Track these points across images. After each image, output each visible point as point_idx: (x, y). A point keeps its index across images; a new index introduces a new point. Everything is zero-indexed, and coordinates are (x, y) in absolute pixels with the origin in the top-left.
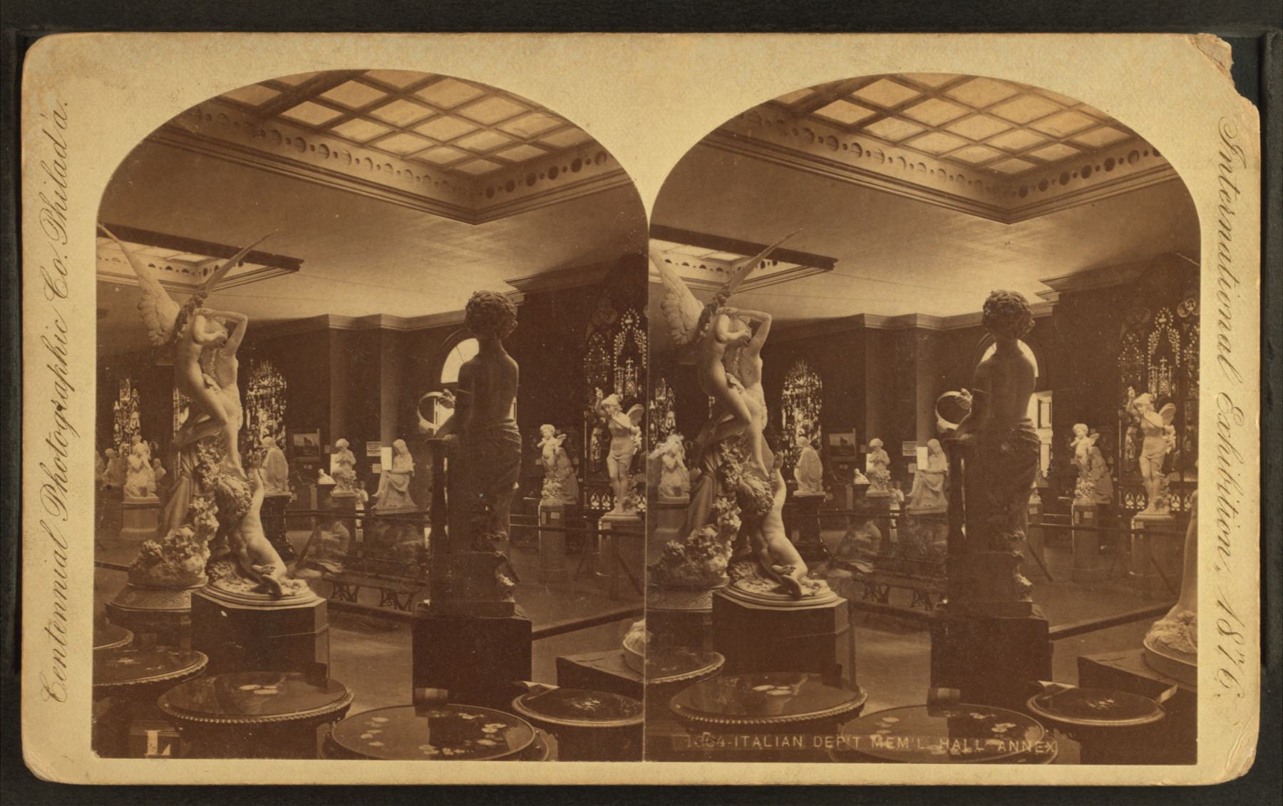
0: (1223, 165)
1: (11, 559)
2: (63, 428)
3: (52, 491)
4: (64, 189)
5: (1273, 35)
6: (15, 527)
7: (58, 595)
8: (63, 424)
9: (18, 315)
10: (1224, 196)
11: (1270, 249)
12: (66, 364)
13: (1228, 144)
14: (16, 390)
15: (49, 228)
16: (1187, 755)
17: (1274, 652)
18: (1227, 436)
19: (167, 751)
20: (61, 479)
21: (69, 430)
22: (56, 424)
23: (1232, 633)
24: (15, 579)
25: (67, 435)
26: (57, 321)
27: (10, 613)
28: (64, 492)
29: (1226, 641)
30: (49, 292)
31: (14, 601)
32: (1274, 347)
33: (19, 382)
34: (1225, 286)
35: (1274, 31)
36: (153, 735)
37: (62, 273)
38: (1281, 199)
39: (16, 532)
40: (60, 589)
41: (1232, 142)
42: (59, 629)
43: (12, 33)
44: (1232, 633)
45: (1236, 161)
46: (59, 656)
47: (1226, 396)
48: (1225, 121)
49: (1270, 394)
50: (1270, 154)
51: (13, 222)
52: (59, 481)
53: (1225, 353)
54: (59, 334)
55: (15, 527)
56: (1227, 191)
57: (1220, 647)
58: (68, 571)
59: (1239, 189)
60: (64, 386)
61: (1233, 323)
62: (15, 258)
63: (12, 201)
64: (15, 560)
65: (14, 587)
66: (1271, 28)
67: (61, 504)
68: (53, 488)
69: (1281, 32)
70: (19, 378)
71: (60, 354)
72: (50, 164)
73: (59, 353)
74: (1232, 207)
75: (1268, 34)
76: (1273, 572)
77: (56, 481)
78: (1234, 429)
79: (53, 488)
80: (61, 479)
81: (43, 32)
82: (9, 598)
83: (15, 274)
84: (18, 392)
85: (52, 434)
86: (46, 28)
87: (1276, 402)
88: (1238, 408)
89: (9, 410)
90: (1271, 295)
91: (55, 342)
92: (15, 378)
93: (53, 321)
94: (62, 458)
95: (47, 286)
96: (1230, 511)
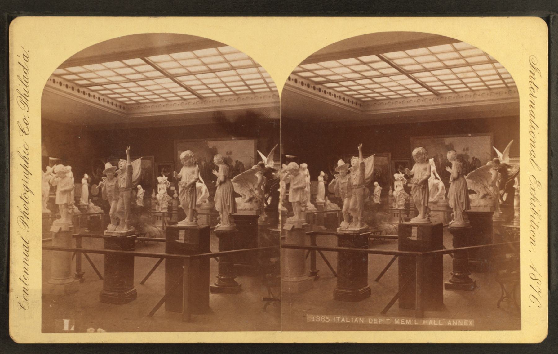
1: (5, 244)
2: (27, 192)
4: (28, 286)
5: (553, 16)
6: (7, 229)
10: (532, 90)
11: (552, 109)
13: (534, 67)
16: (517, 326)
17: (554, 283)
18: (534, 194)
19: (72, 329)
20: (26, 213)
22: (24, 190)
23: (536, 279)
24: (7, 252)
25: (29, 194)
26: (24, 145)
27: (5, 267)
29: (534, 283)
31: (6, 262)
32: (553, 151)
33: (8, 142)
34: (532, 129)
36: (66, 322)
37: (26, 124)
38: (557, 87)
39: (7, 232)
40: (25, 261)
42: (25, 278)
43: (6, 15)
44: (536, 279)
45: (537, 76)
47: (533, 176)
48: (531, 58)
50: (552, 68)
51: (6, 97)
53: (533, 158)
55: (7, 229)
56: (533, 87)
57: (531, 285)
58: (29, 76)
59: (538, 86)
60: (27, 173)
61: (536, 145)
62: (7, 113)
64: (7, 244)
65: (7, 255)
67: (27, 225)
68: (22, 217)
69: (557, 15)
70: (8, 165)
71: (26, 159)
72: (22, 77)
73: (25, 159)
74: (535, 94)
78: (536, 189)
79: (22, 217)
80: (26, 213)
81: (20, 14)
82: (5, 260)
84: (8, 171)
86: (21, 12)
87: (554, 175)
89: (5, 179)
90: (552, 129)
91: (23, 92)
93: (23, 145)
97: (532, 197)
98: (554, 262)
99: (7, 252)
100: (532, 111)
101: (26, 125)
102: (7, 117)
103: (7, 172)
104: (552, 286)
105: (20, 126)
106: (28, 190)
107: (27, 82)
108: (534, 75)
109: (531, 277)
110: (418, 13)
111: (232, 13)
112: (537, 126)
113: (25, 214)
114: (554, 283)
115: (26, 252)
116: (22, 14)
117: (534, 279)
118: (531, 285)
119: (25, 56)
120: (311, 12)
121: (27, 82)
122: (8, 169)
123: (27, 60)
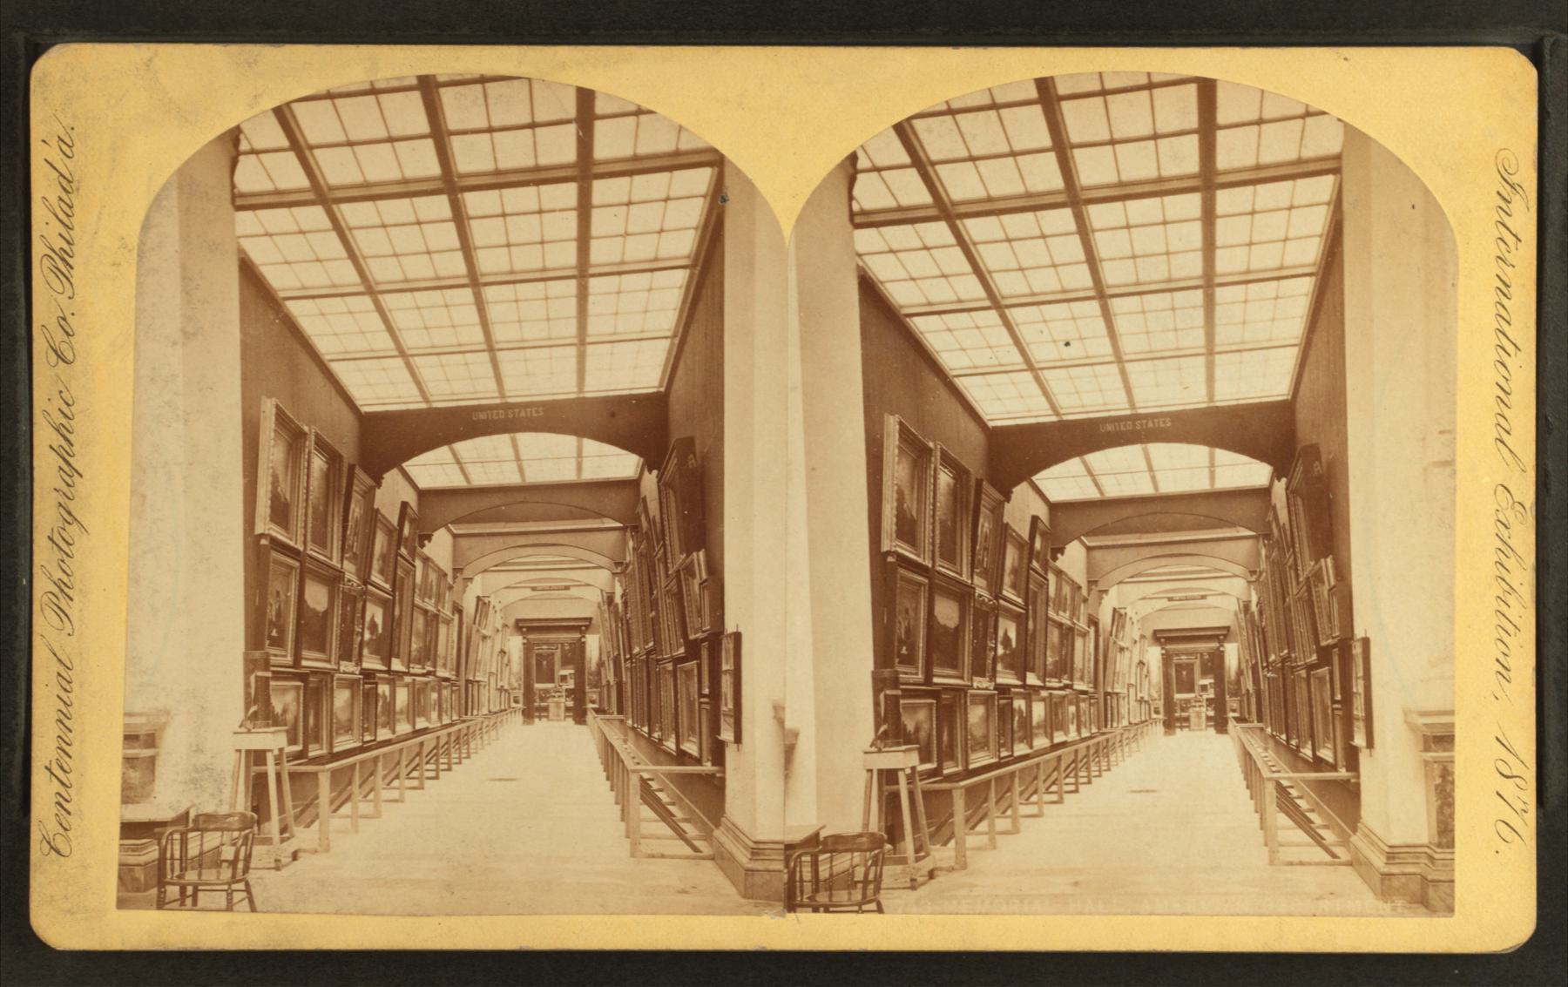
0: (1500, 208)
2: (69, 523)
3: (55, 600)
4: (71, 232)
5: (1552, 40)
7: (62, 727)
8: (69, 519)
9: (27, 382)
12: (72, 445)
14: (25, 473)
15: (52, 278)
17: (1553, 790)
21: (75, 526)
25: (73, 529)
28: (70, 602)
29: (1508, 788)
30: (53, 357)
31: (22, 728)
35: (1552, 36)
37: (68, 334)
41: (1514, 179)
43: (20, 37)
46: (61, 800)
49: (1547, 474)
51: (20, 268)
52: (63, 586)
53: (1505, 436)
54: (65, 408)
57: (1498, 794)
63: (20, 260)
65: (22, 711)
66: (1548, 32)
67: (66, 615)
69: (1563, 37)
70: (28, 457)
71: (66, 256)
72: (53, 200)
73: (63, 431)
74: (1510, 258)
75: (1546, 40)
76: (1551, 690)
77: (59, 587)
81: (58, 37)
82: (17, 725)
83: (22, 331)
85: (55, 531)
87: (1555, 487)
88: (1520, 503)
91: (59, 244)
92: (24, 461)
94: (67, 559)
95: (51, 352)
96: (1510, 348)
97: (1500, 544)
98: (1553, 727)
99: (23, 703)
100: (1503, 306)
101: (65, 338)
102: (23, 325)
103: (24, 479)
104: (1549, 796)
105: (51, 341)
106: (70, 517)
107: (68, 215)
108: (1509, 202)
109: (1501, 773)
110: (1173, 32)
111: (654, 32)
112: (1515, 345)
113: (63, 587)
114: (1553, 790)
115: (64, 695)
116: (64, 35)
117: (1507, 777)
118: (1498, 794)
119: (63, 141)
120: (873, 31)
121: (68, 215)
122: (28, 470)
123: (70, 154)
